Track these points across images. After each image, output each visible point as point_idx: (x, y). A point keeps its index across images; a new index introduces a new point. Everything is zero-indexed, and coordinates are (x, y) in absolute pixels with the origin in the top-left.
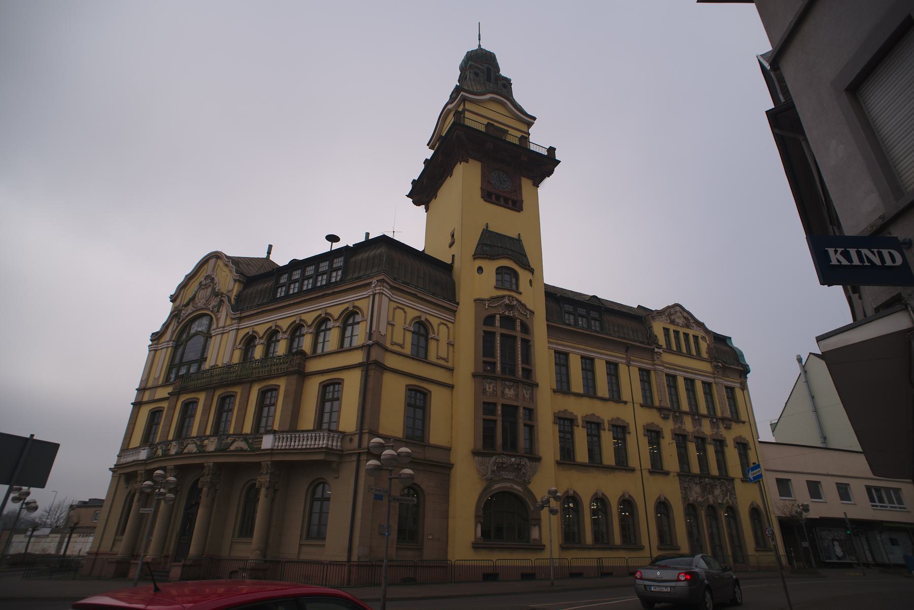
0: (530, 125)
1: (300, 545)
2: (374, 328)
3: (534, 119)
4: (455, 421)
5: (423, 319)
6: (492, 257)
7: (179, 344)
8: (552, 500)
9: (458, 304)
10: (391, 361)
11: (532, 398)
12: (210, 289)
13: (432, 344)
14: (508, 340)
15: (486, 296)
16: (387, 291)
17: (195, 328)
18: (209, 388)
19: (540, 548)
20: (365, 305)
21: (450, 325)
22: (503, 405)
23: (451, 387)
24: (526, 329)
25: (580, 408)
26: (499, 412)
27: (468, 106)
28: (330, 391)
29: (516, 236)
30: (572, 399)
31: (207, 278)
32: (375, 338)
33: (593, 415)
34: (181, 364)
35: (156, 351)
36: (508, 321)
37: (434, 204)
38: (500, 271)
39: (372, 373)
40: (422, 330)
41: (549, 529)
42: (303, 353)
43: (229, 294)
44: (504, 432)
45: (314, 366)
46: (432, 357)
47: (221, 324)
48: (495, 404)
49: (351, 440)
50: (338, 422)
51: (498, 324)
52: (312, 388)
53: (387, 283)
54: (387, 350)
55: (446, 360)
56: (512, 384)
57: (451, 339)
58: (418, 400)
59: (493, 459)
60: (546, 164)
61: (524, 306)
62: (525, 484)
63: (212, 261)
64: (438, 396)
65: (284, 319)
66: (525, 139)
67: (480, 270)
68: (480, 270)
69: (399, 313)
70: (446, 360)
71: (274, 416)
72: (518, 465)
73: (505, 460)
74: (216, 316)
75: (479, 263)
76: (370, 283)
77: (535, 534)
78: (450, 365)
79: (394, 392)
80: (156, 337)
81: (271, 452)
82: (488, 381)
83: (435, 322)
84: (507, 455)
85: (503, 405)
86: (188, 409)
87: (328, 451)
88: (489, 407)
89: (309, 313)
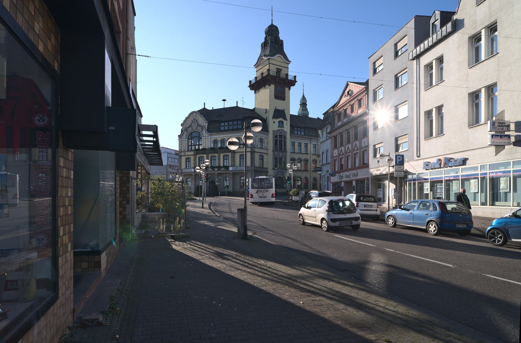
4: (269, 162)
7: (190, 137)
10: (256, 150)
12: (196, 124)
13: (263, 144)
14: (281, 142)
24: (285, 138)
25: (296, 156)
31: (194, 119)
34: (191, 146)
36: (281, 136)
38: (279, 122)
46: (264, 147)
58: (262, 158)
60: (293, 83)
62: (283, 175)
63: (194, 114)
64: (265, 156)
66: (287, 75)
68: (274, 122)
75: (274, 120)
77: (285, 186)
80: (180, 136)
81: (232, 170)
83: (264, 138)
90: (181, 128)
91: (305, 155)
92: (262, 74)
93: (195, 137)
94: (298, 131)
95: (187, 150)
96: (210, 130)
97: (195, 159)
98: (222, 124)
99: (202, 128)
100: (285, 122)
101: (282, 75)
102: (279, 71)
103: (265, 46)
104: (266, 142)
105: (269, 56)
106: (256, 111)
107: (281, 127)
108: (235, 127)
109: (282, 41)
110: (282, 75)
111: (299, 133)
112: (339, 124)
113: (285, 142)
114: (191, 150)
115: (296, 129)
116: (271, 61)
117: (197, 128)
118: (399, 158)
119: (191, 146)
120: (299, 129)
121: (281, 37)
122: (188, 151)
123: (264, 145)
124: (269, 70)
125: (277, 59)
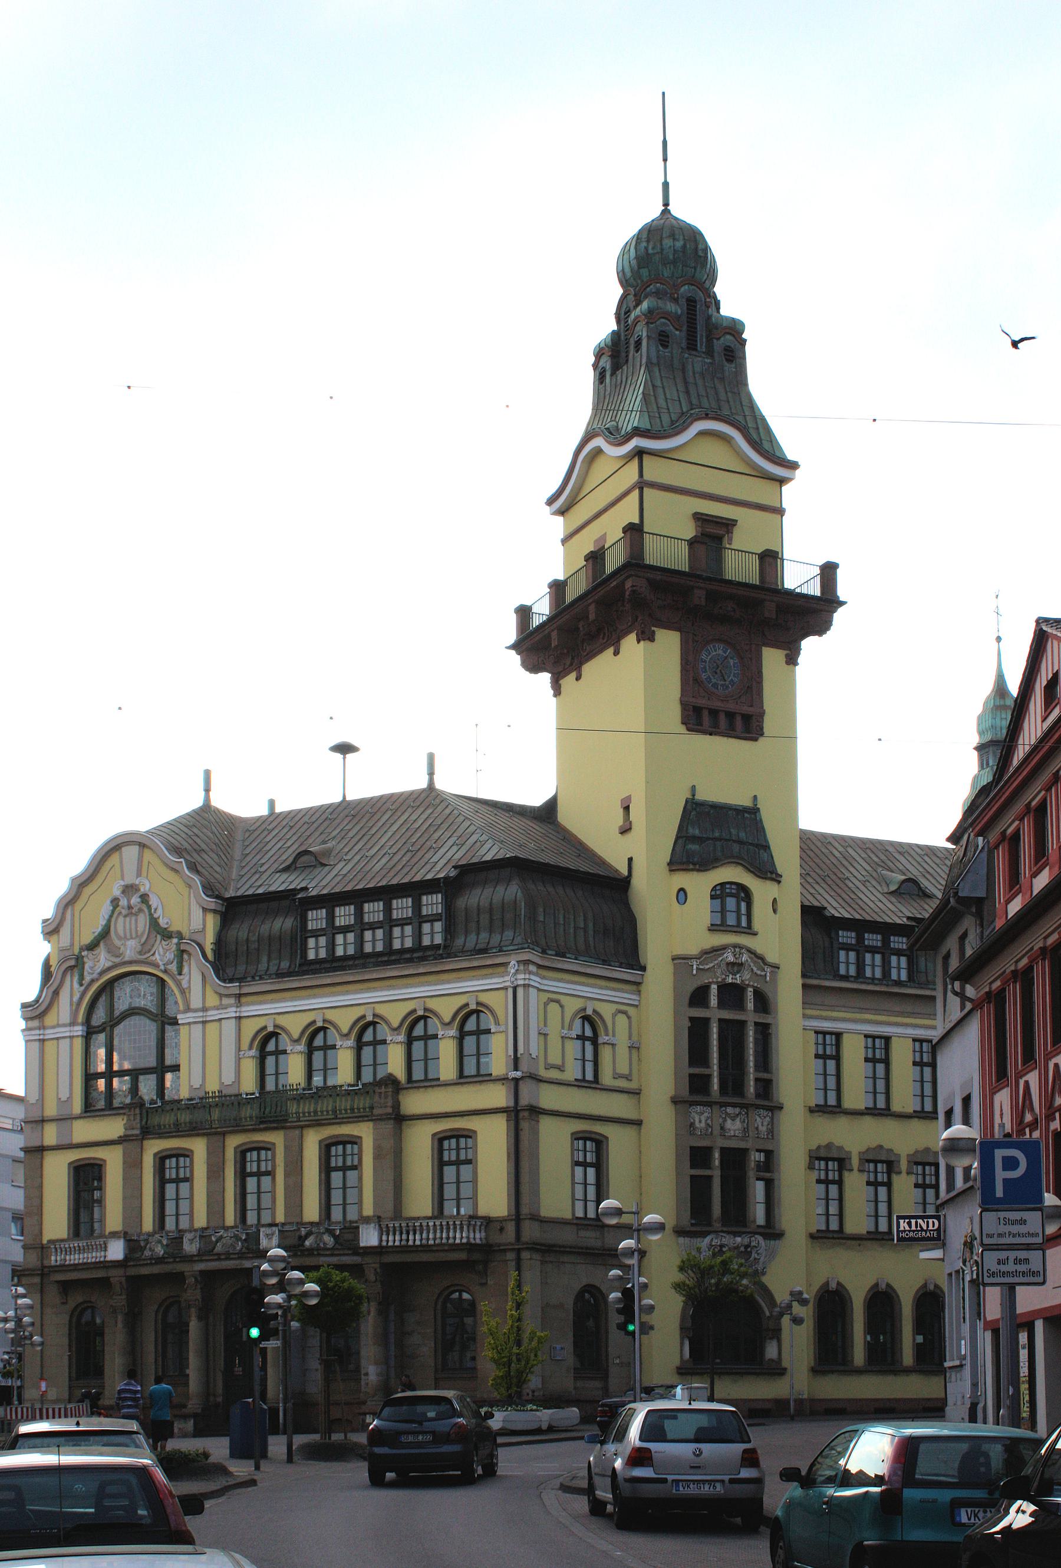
0: (782, 481)
1: (436, 1379)
2: (521, 1050)
3: (793, 466)
4: (646, 1182)
5: (589, 1012)
6: (703, 865)
7: (100, 1021)
8: (795, 1304)
9: (643, 969)
10: (549, 1098)
11: (772, 1132)
12: (143, 921)
13: (606, 1053)
14: (733, 1032)
15: (694, 951)
16: (535, 981)
17: (125, 997)
18: (215, 1134)
19: (777, 1370)
20: (500, 1003)
21: (631, 1011)
22: (723, 1150)
23: (638, 1123)
24: (763, 1003)
25: (854, 1137)
26: (717, 1163)
27: (655, 470)
28: (453, 1149)
29: (748, 803)
30: (843, 1121)
31: (129, 889)
32: (524, 1066)
33: (881, 1147)
35: (42, 1041)
36: (732, 995)
37: (569, 682)
38: (720, 893)
39: (524, 1125)
40: (591, 1029)
41: (796, 1344)
42: (391, 1081)
43: (198, 938)
44: (722, 1187)
45: (414, 1102)
46: (607, 1079)
47: (196, 1002)
48: (709, 1150)
49: (502, 1229)
50: (474, 1198)
51: (714, 1001)
52: (419, 1143)
53: (534, 963)
54: (540, 1080)
55: (628, 1078)
56: (737, 1110)
57: (635, 1038)
58: (592, 1153)
59: (707, 1239)
60: (815, 612)
61: (762, 958)
63: (131, 853)
64: (618, 1140)
65: (341, 1004)
66: (771, 559)
67: (682, 894)
68: (682, 894)
69: (553, 1007)
70: (628, 1078)
71: (360, 1188)
72: (747, 1247)
73: (725, 1241)
74: (178, 984)
75: (683, 879)
76: (505, 965)
77: (771, 1351)
78: (633, 1085)
79: (554, 1142)
80: (35, 1013)
81: (379, 1251)
82: (699, 1108)
83: (606, 1011)
84: (728, 1233)
85: (723, 1150)
86: (170, 1173)
87: (470, 1247)
88: (699, 1156)
89: (392, 999)
90: (45, 948)
91: (868, 1123)
92: (596, 558)
93: (132, 1012)
94: (860, 948)
95: (77, 1107)
96: (230, 963)
97: (133, 1166)
98: (316, 919)
99: (181, 953)
100: (762, 891)
101: (738, 566)
102: (712, 533)
103: (616, 367)
104: (622, 1039)
105: (637, 432)
106: (564, 817)
107: (737, 929)
108: (403, 938)
109: (735, 330)
110: (738, 566)
111: (873, 965)
112: (1015, 907)
113: (765, 1032)
114: (110, 1108)
115: (847, 937)
116: (655, 470)
117: (145, 948)
118: (1010, 1163)
119: (109, 1074)
120: (873, 939)
121: (732, 297)
122: (89, 1109)
123: (614, 1062)
124: (634, 531)
125: (701, 456)
